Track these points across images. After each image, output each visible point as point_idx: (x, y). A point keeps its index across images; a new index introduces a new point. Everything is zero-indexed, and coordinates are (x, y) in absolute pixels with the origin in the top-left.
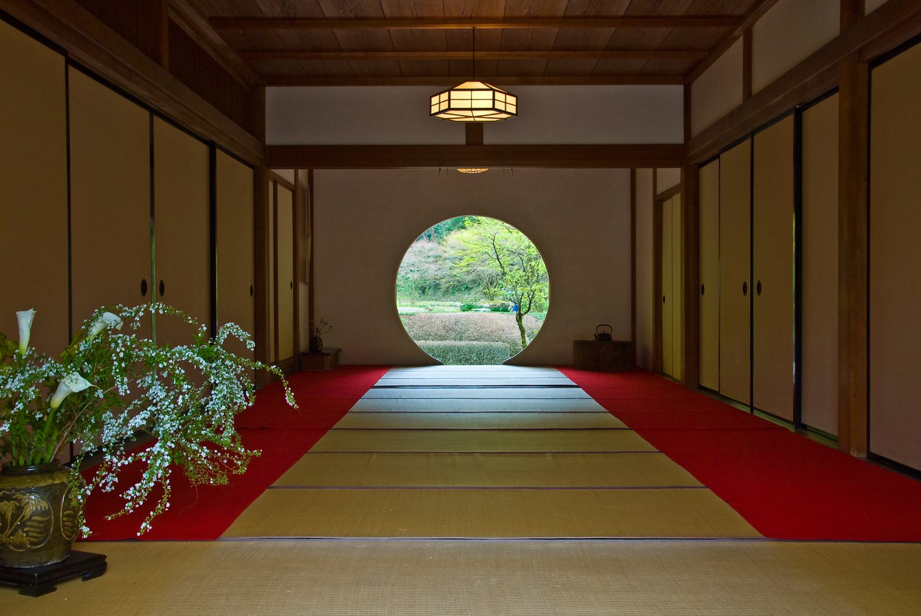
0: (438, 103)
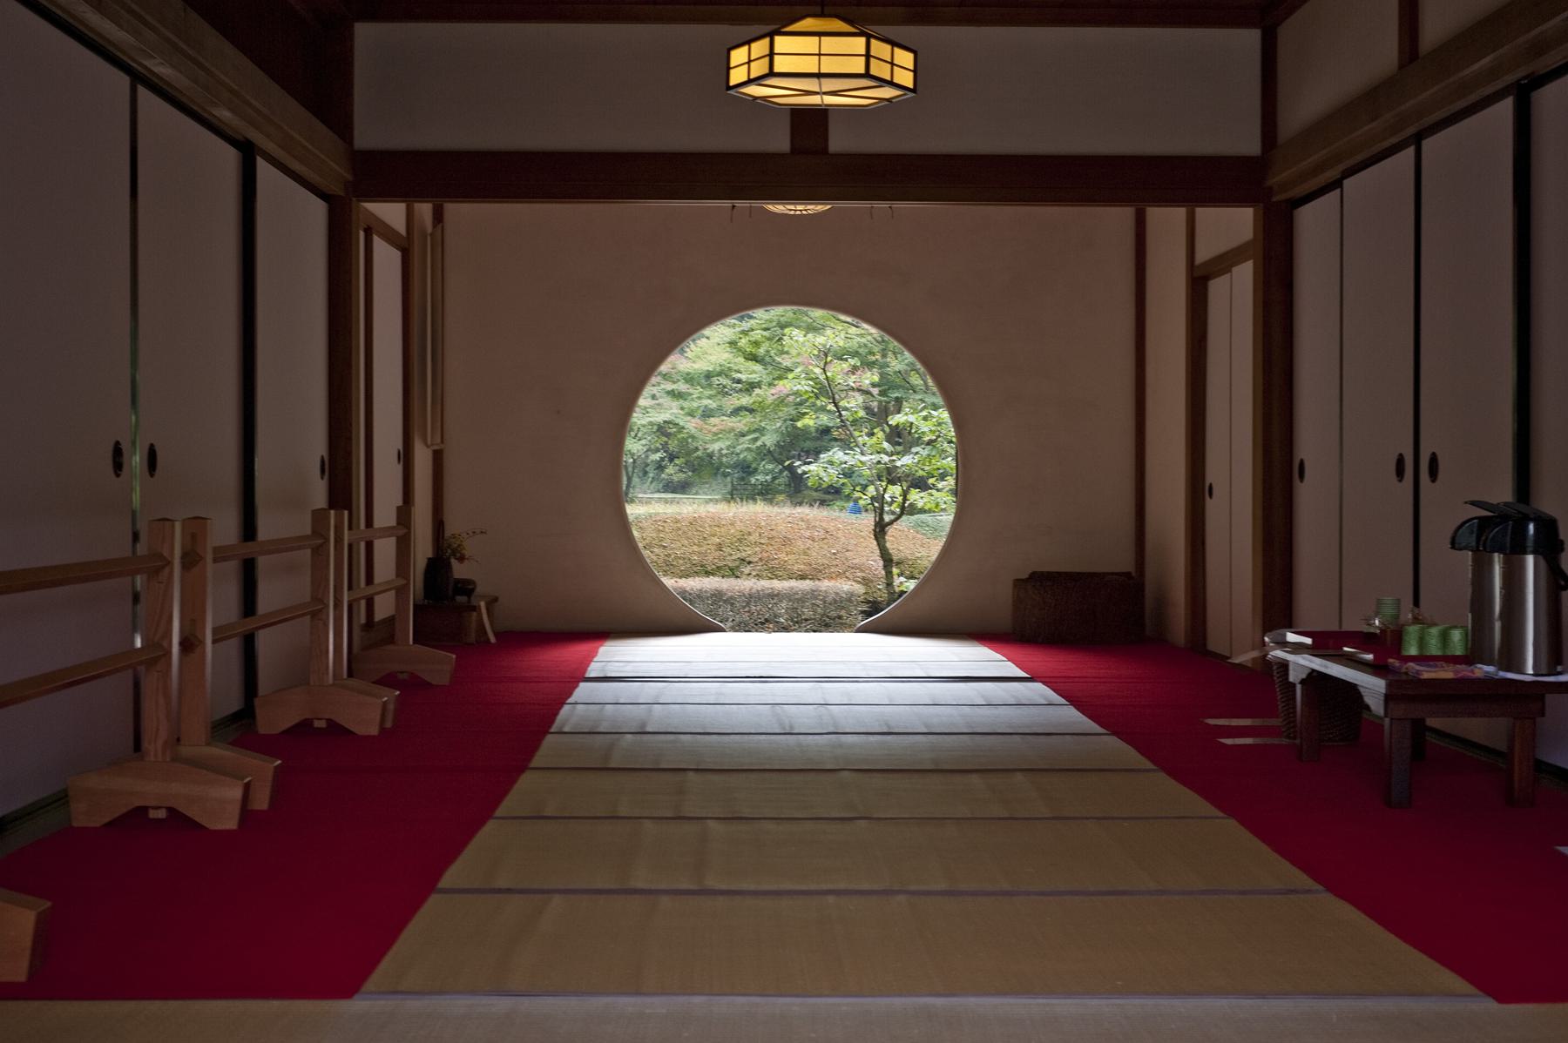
0: (742, 63)
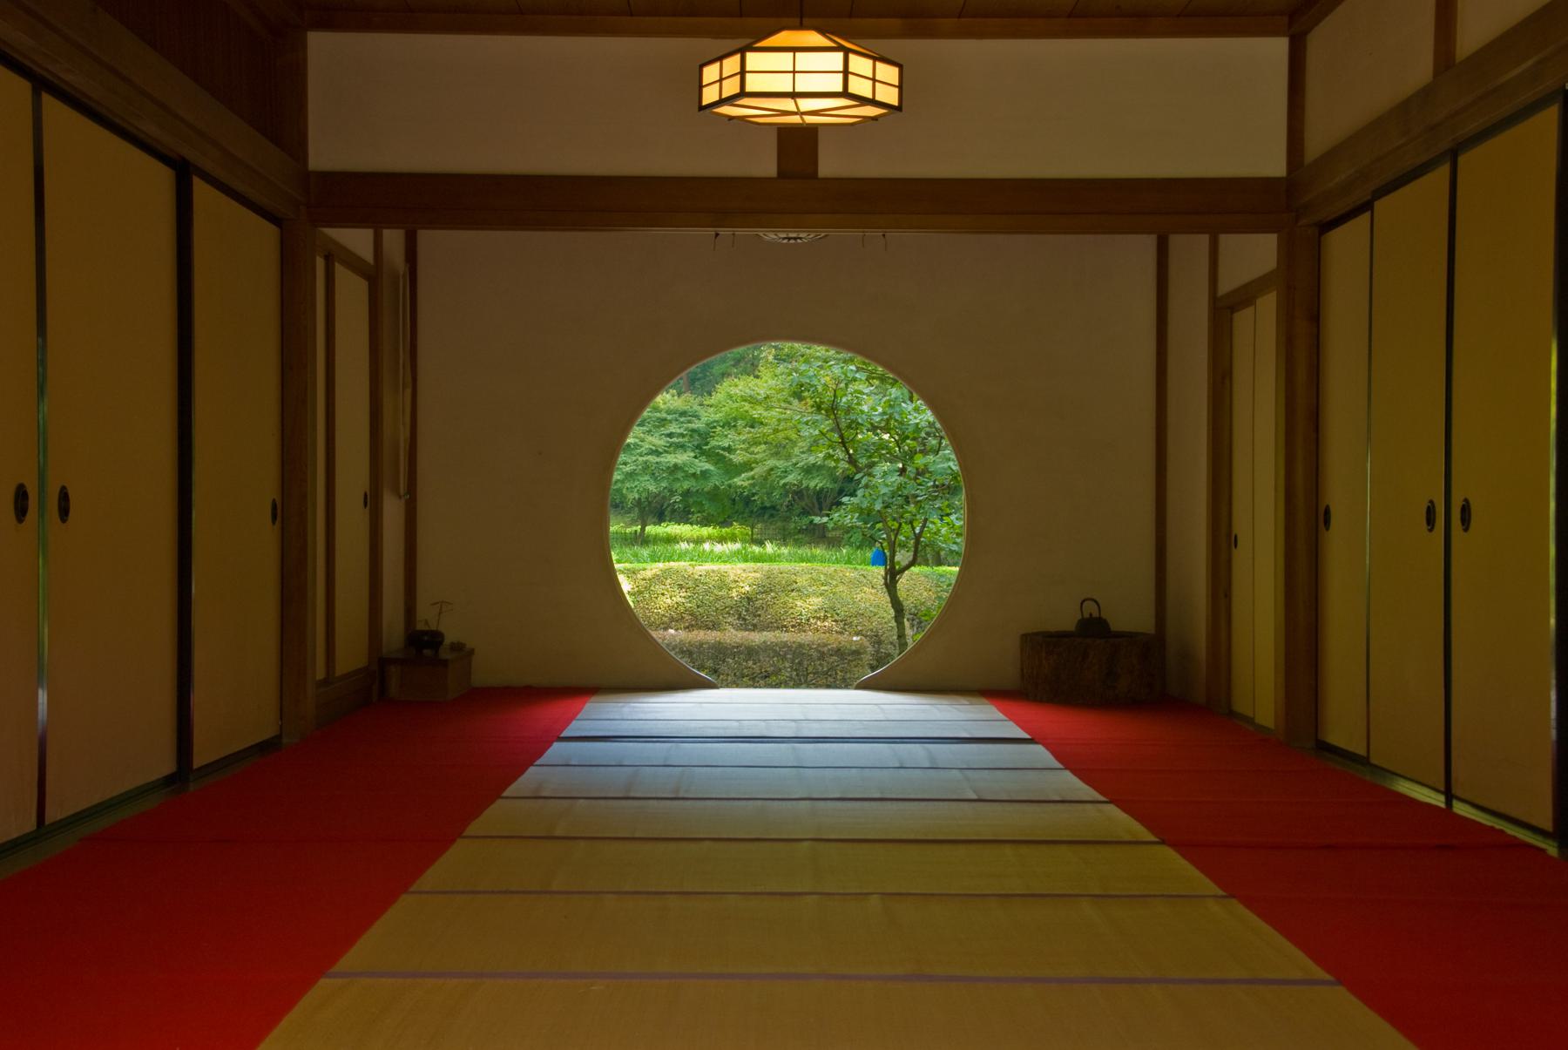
0: (716, 80)
